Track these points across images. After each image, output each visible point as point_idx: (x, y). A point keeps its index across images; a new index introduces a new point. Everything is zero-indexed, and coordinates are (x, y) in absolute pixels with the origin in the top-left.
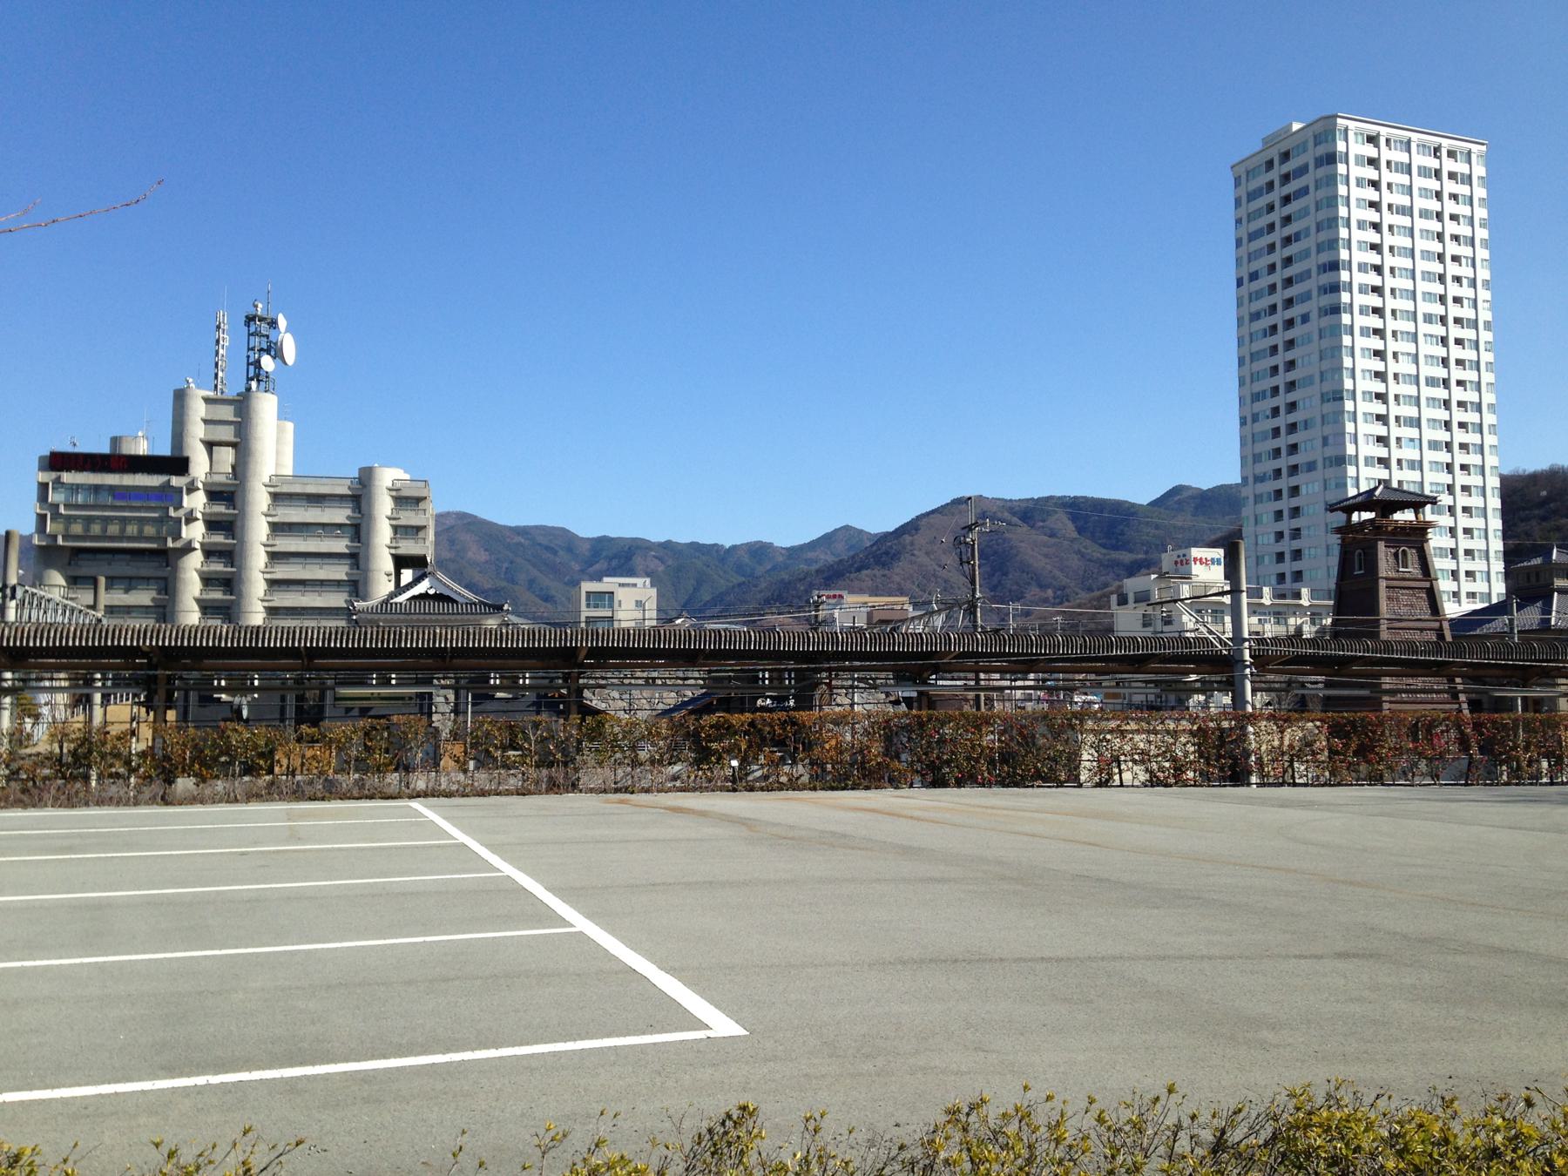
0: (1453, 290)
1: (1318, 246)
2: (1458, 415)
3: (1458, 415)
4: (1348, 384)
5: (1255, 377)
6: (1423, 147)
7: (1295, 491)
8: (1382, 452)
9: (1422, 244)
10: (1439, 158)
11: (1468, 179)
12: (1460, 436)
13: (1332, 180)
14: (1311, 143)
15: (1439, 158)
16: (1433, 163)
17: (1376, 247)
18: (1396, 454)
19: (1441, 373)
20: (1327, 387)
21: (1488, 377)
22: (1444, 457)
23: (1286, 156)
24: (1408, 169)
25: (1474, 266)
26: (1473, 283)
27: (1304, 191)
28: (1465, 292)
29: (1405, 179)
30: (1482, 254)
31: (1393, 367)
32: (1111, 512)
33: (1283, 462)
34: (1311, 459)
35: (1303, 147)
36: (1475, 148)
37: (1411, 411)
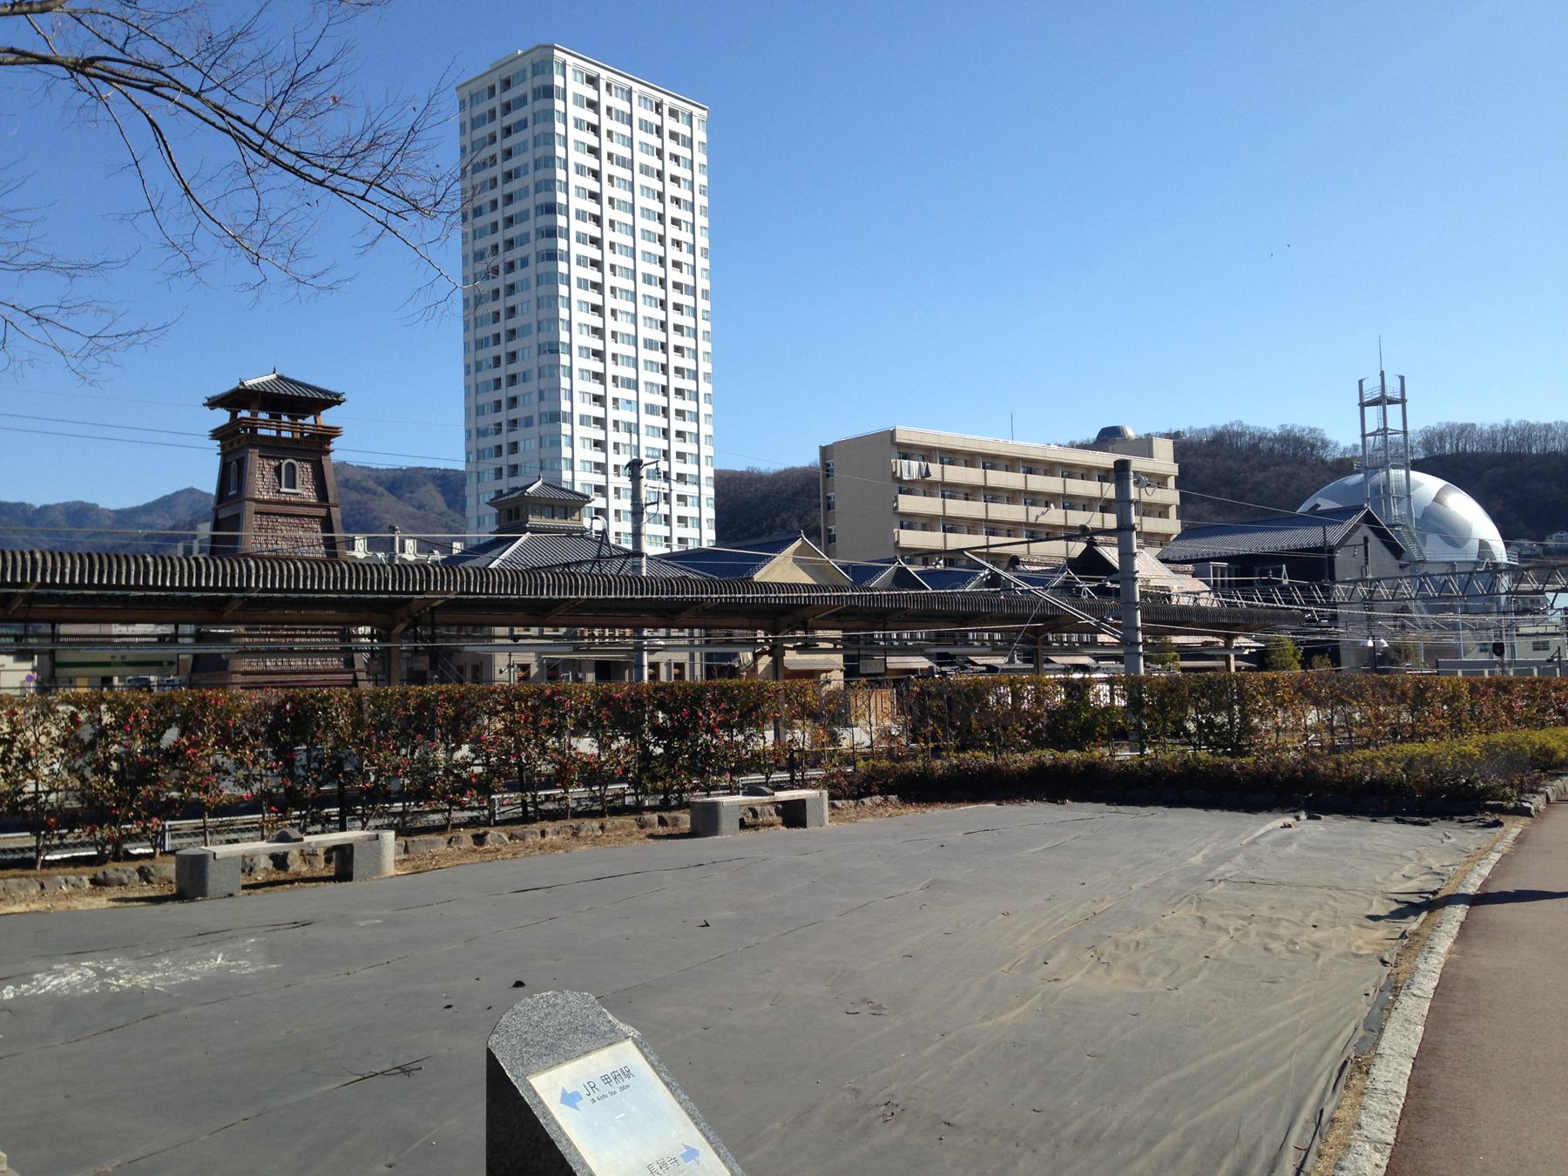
0: (673, 254)
1: (536, 185)
2: (676, 382)
3: (676, 382)
4: (564, 337)
5: (479, 300)
6: (644, 98)
7: (514, 447)
8: (598, 412)
9: (642, 202)
10: (661, 114)
11: (689, 142)
12: (676, 403)
13: (549, 115)
14: (529, 74)
15: (661, 114)
16: (655, 119)
17: (595, 196)
18: (613, 414)
19: (659, 336)
20: (544, 338)
21: (706, 408)
22: (660, 422)
23: (507, 84)
24: (629, 120)
25: (693, 232)
26: (692, 249)
27: (522, 125)
28: (684, 257)
29: (625, 129)
30: (702, 221)
31: (611, 326)
32: (328, 818)
33: (504, 416)
34: (527, 414)
35: (521, 76)
36: (696, 111)
37: (629, 373)
